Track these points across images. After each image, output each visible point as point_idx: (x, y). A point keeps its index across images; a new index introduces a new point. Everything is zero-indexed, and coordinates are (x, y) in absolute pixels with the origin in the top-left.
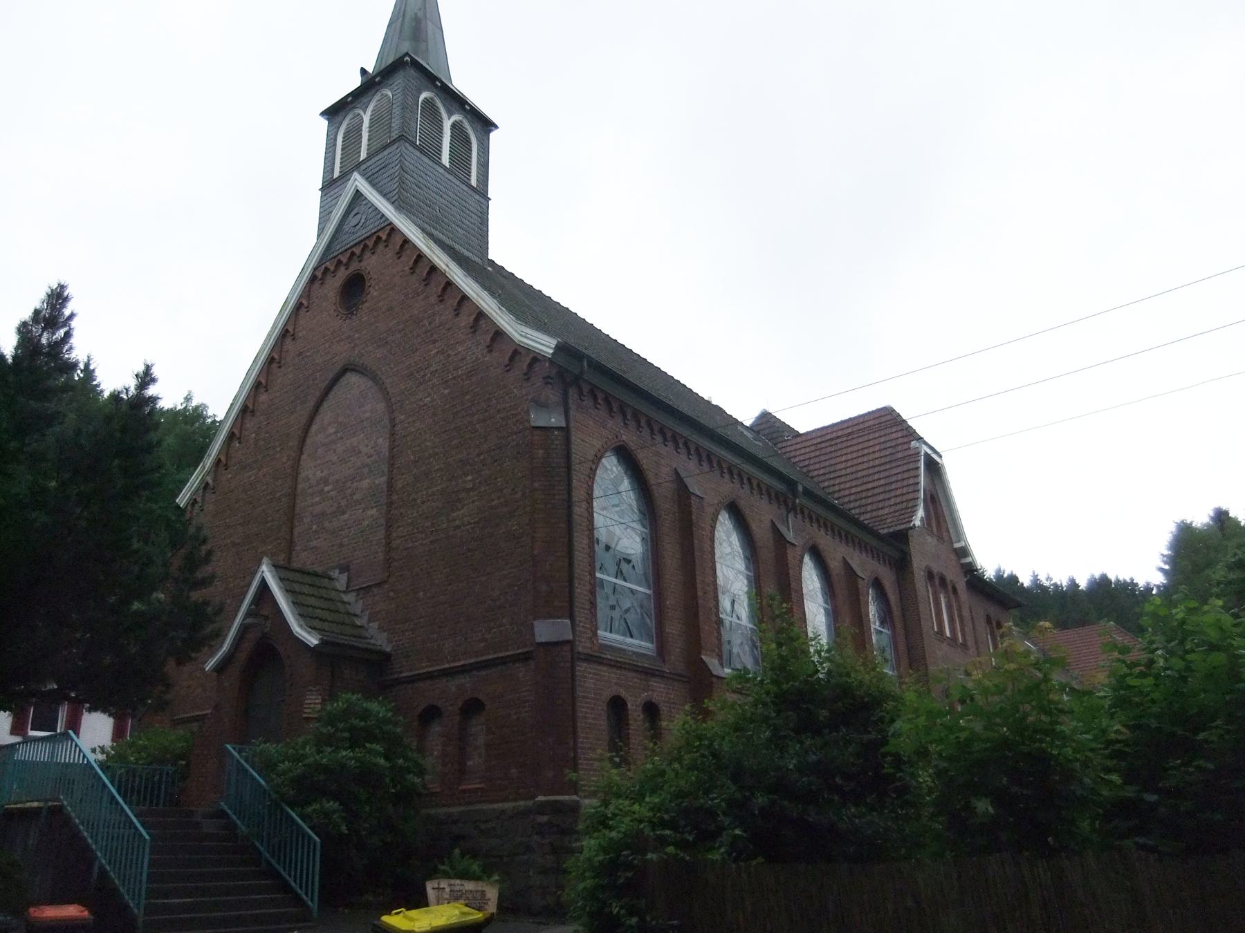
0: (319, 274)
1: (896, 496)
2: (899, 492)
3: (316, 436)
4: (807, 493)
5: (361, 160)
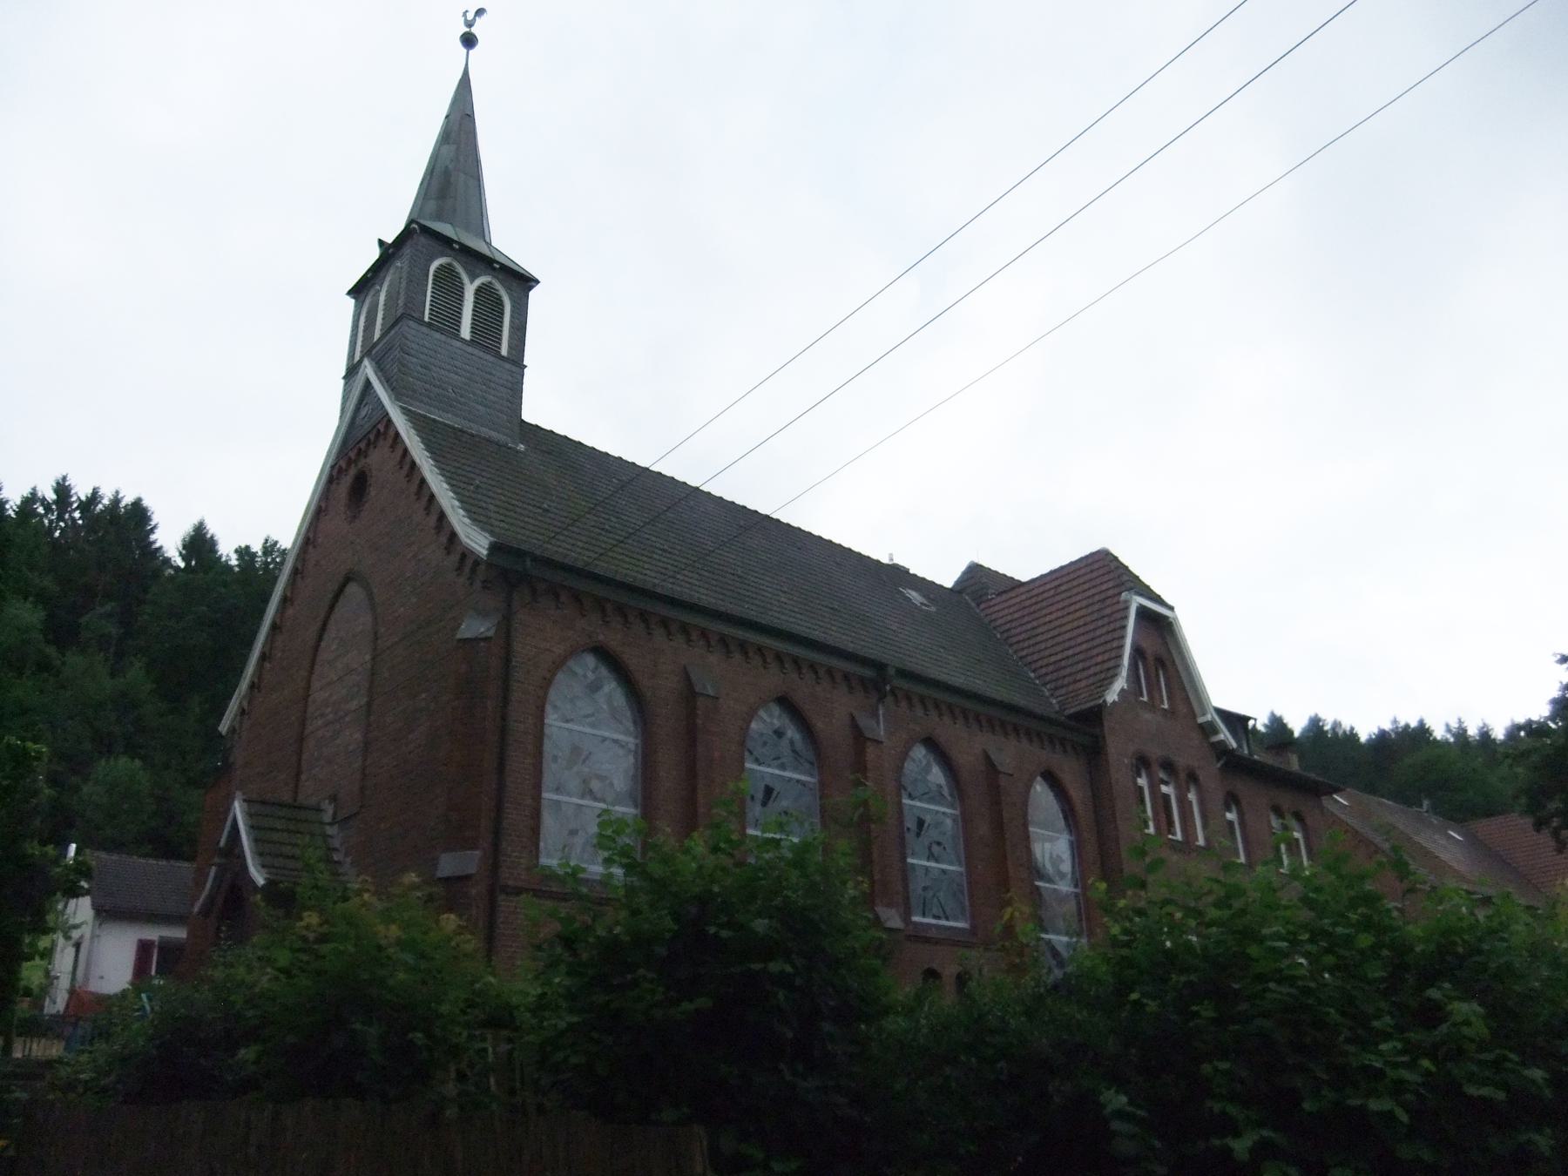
0: (335, 473)
1: (1097, 664)
2: (1100, 659)
3: (323, 656)
4: (904, 674)
5: (375, 340)
